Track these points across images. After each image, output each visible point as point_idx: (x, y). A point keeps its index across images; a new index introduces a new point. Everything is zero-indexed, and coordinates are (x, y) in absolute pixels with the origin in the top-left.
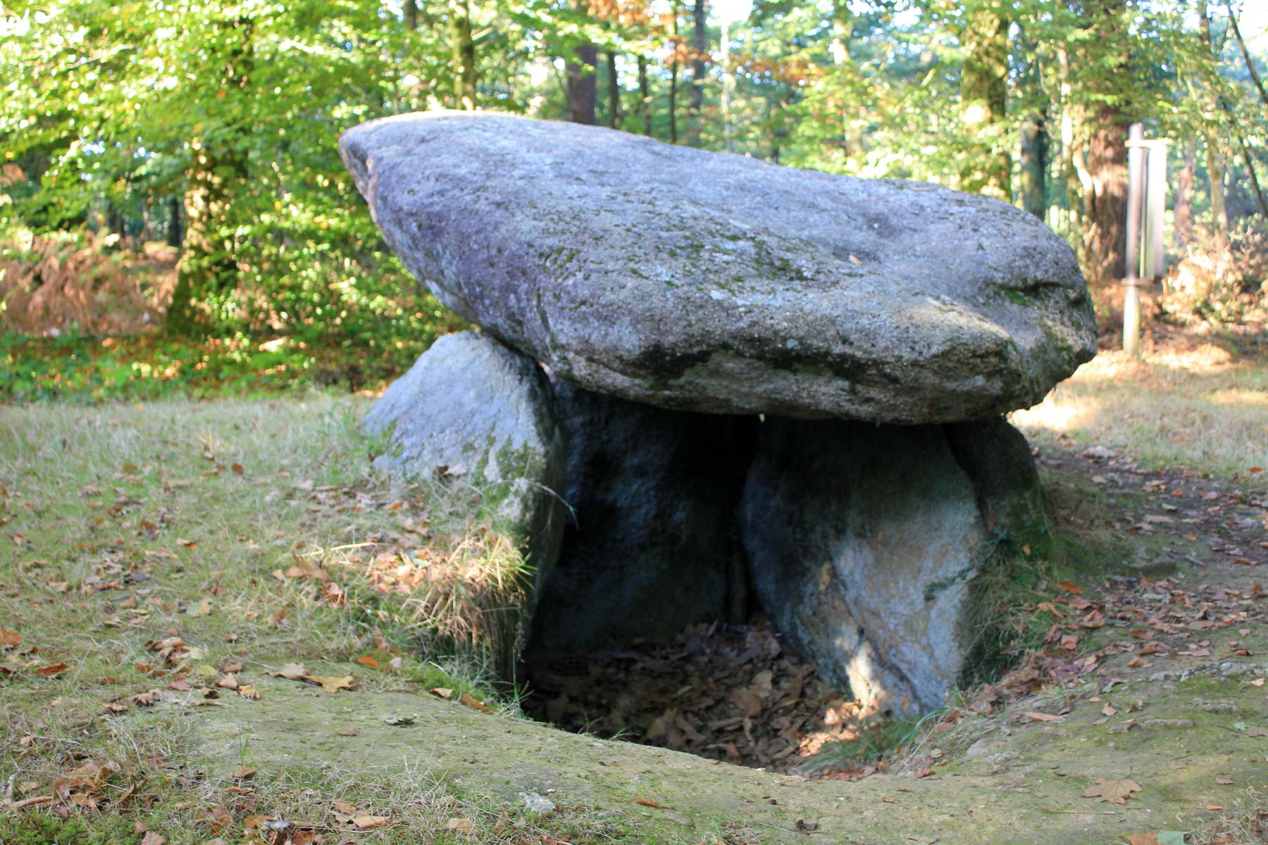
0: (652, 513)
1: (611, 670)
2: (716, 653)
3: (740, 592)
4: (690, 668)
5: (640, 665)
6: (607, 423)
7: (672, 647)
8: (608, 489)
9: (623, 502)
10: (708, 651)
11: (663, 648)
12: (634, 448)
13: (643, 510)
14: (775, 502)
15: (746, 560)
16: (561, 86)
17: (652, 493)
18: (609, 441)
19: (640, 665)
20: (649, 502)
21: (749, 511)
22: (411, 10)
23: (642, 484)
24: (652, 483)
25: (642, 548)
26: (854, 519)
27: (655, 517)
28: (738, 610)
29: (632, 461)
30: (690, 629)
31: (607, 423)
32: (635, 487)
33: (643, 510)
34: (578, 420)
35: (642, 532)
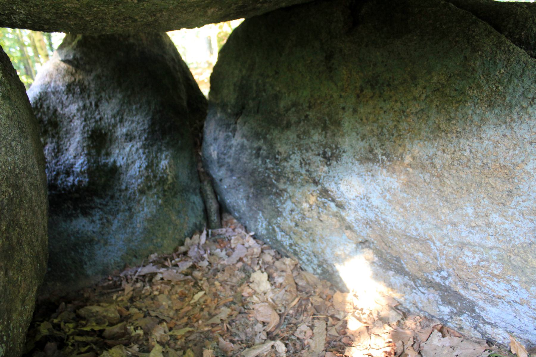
0: (144, 166)
1: (139, 285)
2: (211, 254)
3: (213, 206)
4: (197, 274)
5: (159, 276)
6: (97, 106)
7: (178, 256)
8: (108, 154)
9: (120, 162)
10: (205, 256)
11: (172, 259)
12: (121, 121)
13: (137, 164)
14: (237, 140)
15: (212, 182)
17: (141, 151)
18: (101, 119)
19: (159, 276)
20: (140, 158)
21: (213, 151)
22: (13, 1)
23: (133, 146)
24: (139, 144)
25: (142, 192)
26: (350, 143)
27: (147, 168)
28: (214, 218)
29: (121, 131)
30: (188, 241)
31: (97, 106)
32: (127, 149)
33: (137, 164)
34: (74, 108)
35: (139, 181)
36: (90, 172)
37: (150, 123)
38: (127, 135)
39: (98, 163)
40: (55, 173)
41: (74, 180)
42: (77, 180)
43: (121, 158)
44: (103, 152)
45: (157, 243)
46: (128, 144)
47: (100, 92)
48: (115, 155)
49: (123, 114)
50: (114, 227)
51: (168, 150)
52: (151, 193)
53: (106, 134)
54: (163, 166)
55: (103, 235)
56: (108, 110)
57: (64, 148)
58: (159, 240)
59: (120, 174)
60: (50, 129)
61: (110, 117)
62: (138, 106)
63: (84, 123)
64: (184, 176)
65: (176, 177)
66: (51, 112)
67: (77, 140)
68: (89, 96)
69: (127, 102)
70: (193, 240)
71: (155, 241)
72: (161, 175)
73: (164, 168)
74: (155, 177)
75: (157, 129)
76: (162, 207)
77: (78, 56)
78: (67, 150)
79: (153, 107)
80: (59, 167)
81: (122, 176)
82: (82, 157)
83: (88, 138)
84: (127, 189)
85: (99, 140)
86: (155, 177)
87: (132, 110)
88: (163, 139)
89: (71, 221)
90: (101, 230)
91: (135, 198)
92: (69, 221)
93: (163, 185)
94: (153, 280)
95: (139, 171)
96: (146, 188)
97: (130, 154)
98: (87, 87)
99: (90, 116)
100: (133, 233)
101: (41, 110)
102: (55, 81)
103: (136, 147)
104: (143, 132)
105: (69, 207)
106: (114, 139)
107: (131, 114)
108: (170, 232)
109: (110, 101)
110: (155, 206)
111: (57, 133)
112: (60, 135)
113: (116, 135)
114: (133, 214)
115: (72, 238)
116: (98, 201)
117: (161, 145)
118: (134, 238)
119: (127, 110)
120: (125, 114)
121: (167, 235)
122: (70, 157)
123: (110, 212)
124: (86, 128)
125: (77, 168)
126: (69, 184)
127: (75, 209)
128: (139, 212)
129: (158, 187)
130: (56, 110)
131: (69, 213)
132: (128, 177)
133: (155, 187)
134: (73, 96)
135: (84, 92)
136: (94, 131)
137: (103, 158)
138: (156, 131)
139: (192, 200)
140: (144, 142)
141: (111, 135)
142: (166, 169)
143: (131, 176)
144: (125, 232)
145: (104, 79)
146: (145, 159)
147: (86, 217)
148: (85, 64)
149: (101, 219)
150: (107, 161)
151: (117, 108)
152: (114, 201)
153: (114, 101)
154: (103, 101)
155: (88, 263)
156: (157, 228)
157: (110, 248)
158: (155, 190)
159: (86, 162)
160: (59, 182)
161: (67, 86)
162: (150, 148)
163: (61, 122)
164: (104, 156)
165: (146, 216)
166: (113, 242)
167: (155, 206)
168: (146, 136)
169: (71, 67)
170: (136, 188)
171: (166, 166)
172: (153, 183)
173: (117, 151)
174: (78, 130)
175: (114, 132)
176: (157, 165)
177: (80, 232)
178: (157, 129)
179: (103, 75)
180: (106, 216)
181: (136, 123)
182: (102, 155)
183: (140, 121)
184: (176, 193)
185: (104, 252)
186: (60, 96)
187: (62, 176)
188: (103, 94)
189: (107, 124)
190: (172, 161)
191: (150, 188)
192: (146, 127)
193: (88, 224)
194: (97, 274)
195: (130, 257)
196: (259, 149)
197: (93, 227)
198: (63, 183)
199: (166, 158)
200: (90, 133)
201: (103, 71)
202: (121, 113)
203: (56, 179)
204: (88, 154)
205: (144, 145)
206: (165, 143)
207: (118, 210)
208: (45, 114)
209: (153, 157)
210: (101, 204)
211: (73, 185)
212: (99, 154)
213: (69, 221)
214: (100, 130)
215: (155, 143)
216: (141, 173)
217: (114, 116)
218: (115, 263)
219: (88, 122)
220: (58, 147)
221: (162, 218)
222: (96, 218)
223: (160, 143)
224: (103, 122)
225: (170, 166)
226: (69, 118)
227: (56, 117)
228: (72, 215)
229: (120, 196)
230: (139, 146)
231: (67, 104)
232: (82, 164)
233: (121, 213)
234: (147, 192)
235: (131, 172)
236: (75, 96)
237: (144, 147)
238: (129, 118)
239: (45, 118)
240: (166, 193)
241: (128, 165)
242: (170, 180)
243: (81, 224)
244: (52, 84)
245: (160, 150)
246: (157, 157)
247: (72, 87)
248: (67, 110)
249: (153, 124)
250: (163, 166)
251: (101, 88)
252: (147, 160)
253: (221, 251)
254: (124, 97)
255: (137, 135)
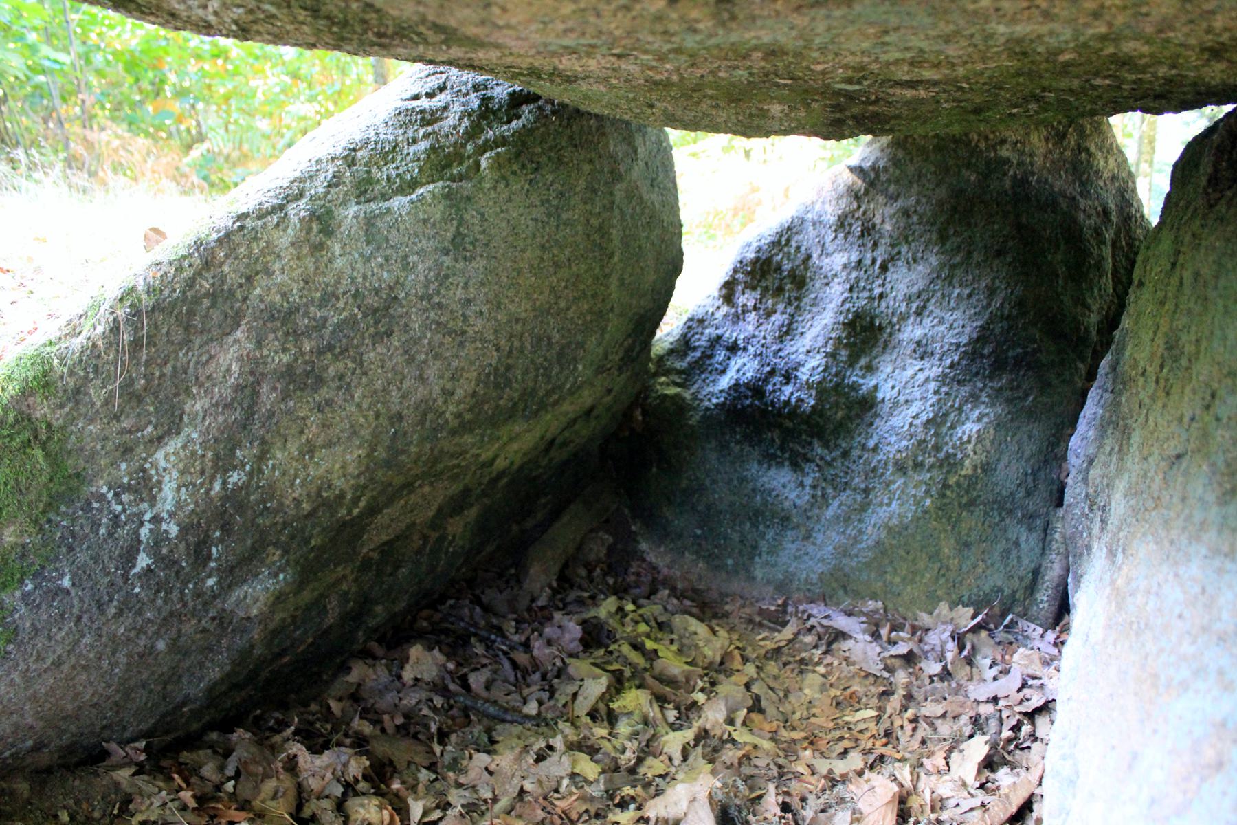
0: (924, 417)
8: (870, 369)
12: (919, 313)
13: (914, 409)
16: (1120, 382)
17: (932, 386)
18: (881, 296)
20: (924, 398)
24: (936, 371)
25: (901, 468)
29: (912, 332)
30: (943, 608)
31: (884, 268)
32: (910, 372)
33: (914, 409)
35: (904, 443)
36: (821, 390)
37: (975, 335)
38: (919, 343)
39: (843, 380)
40: (768, 369)
41: (792, 394)
42: (796, 395)
43: (891, 385)
44: (863, 361)
45: (891, 583)
46: (915, 362)
47: (900, 244)
48: (883, 376)
49: (928, 300)
50: (829, 513)
51: (993, 405)
52: (916, 477)
53: (881, 328)
54: (964, 433)
55: (808, 518)
56: (904, 282)
57: (800, 330)
58: (897, 580)
59: (876, 415)
60: (788, 286)
61: (900, 297)
62: (967, 291)
63: (846, 295)
64: (1010, 473)
65: (987, 468)
66: (801, 256)
67: (825, 322)
68: (875, 245)
69: (946, 276)
70: (953, 614)
71: (888, 577)
72: (951, 451)
73: (965, 438)
74: (937, 448)
75: (986, 352)
76: (927, 516)
77: (881, 164)
78: (802, 334)
79: (997, 303)
80: (778, 360)
81: (877, 422)
82: (818, 357)
83: (844, 324)
84: (875, 449)
85: (864, 334)
86: (937, 448)
87: (949, 296)
88: (991, 378)
89: (769, 468)
90: (808, 507)
91: (883, 474)
92: (765, 466)
93: (948, 472)
94: (834, 646)
95: (911, 425)
96: (911, 463)
97: (910, 385)
98: (877, 227)
99: (862, 284)
100: (856, 540)
101: (786, 249)
102: (823, 203)
103: (927, 373)
104: (953, 348)
105: (773, 440)
106: (893, 343)
107: (945, 304)
108: (928, 576)
109: (913, 266)
110: (913, 508)
111: (798, 299)
112: (802, 304)
113: (901, 336)
114: (869, 504)
115: (758, 498)
116: (819, 451)
117: (981, 390)
118: (855, 551)
119: (939, 294)
120: (933, 301)
121: (917, 579)
122: (800, 350)
123: (832, 482)
124: (847, 306)
125: (803, 374)
126: (783, 398)
127: (783, 449)
128: (881, 505)
129: (935, 472)
130: (809, 257)
131: (772, 451)
132: (886, 428)
133: (929, 471)
134: (846, 238)
135: (869, 235)
136: (857, 316)
137: (858, 371)
138: (982, 356)
139: (1012, 535)
140: (948, 370)
141: (891, 334)
142: (969, 442)
143: (893, 428)
144: (843, 533)
145: (915, 218)
146: (933, 405)
147: (795, 471)
148: (889, 181)
149: (814, 487)
150: (861, 381)
151: (921, 285)
152: (846, 463)
153: (920, 268)
154: (900, 263)
155: (764, 556)
156: (902, 553)
157: (811, 549)
158: (928, 475)
159: (821, 369)
160: (770, 387)
161: (839, 217)
162: (956, 387)
163: (812, 279)
164: (861, 368)
165: (890, 519)
166: (818, 542)
167: (913, 508)
168: (956, 358)
169: (860, 182)
170: (891, 456)
171: (970, 437)
172: (930, 461)
173: (889, 369)
174: (832, 306)
175: (899, 330)
176: (952, 427)
177: (774, 493)
178: (986, 352)
179: (915, 211)
180: (824, 485)
181: (949, 326)
182: (858, 366)
183: (956, 325)
184: (972, 503)
185: (798, 550)
186: (823, 232)
187: (777, 379)
188: (904, 249)
189: (890, 311)
190: (992, 431)
191: (918, 466)
192: (964, 339)
193: (792, 485)
194: (768, 582)
195: (835, 585)
196: (1031, 431)
197: (798, 496)
198: (774, 391)
199: (979, 420)
200: (850, 316)
201: (918, 202)
202: (924, 296)
203: (766, 381)
204: (833, 355)
205: (945, 375)
206: (991, 388)
207: (846, 483)
208: (788, 259)
209: (952, 406)
210: (822, 458)
211: (787, 402)
212: (853, 361)
213: (765, 466)
214: (873, 318)
215: (970, 380)
216: (912, 429)
217: (909, 299)
218: (806, 580)
219: (855, 296)
220: (790, 325)
221: (919, 538)
222: (808, 481)
223: (980, 385)
224: (883, 304)
225: (980, 439)
226: (826, 277)
227: (806, 269)
228: (774, 456)
229: (860, 457)
230: (932, 375)
231: (831, 249)
232: (814, 368)
233: (848, 492)
234: (910, 473)
235: (896, 421)
236: (850, 238)
237: (942, 379)
238: (937, 312)
239: (787, 266)
240: (948, 493)
241: (896, 404)
242: (967, 469)
243: (782, 481)
244: (818, 207)
245: (974, 398)
246: (960, 409)
247: (850, 220)
248: (826, 261)
249: (982, 338)
250: (964, 433)
251: (904, 236)
252: (936, 408)
253: (991, 667)
254: (942, 265)
255: (938, 350)
